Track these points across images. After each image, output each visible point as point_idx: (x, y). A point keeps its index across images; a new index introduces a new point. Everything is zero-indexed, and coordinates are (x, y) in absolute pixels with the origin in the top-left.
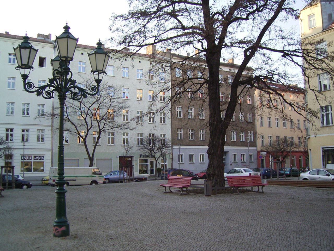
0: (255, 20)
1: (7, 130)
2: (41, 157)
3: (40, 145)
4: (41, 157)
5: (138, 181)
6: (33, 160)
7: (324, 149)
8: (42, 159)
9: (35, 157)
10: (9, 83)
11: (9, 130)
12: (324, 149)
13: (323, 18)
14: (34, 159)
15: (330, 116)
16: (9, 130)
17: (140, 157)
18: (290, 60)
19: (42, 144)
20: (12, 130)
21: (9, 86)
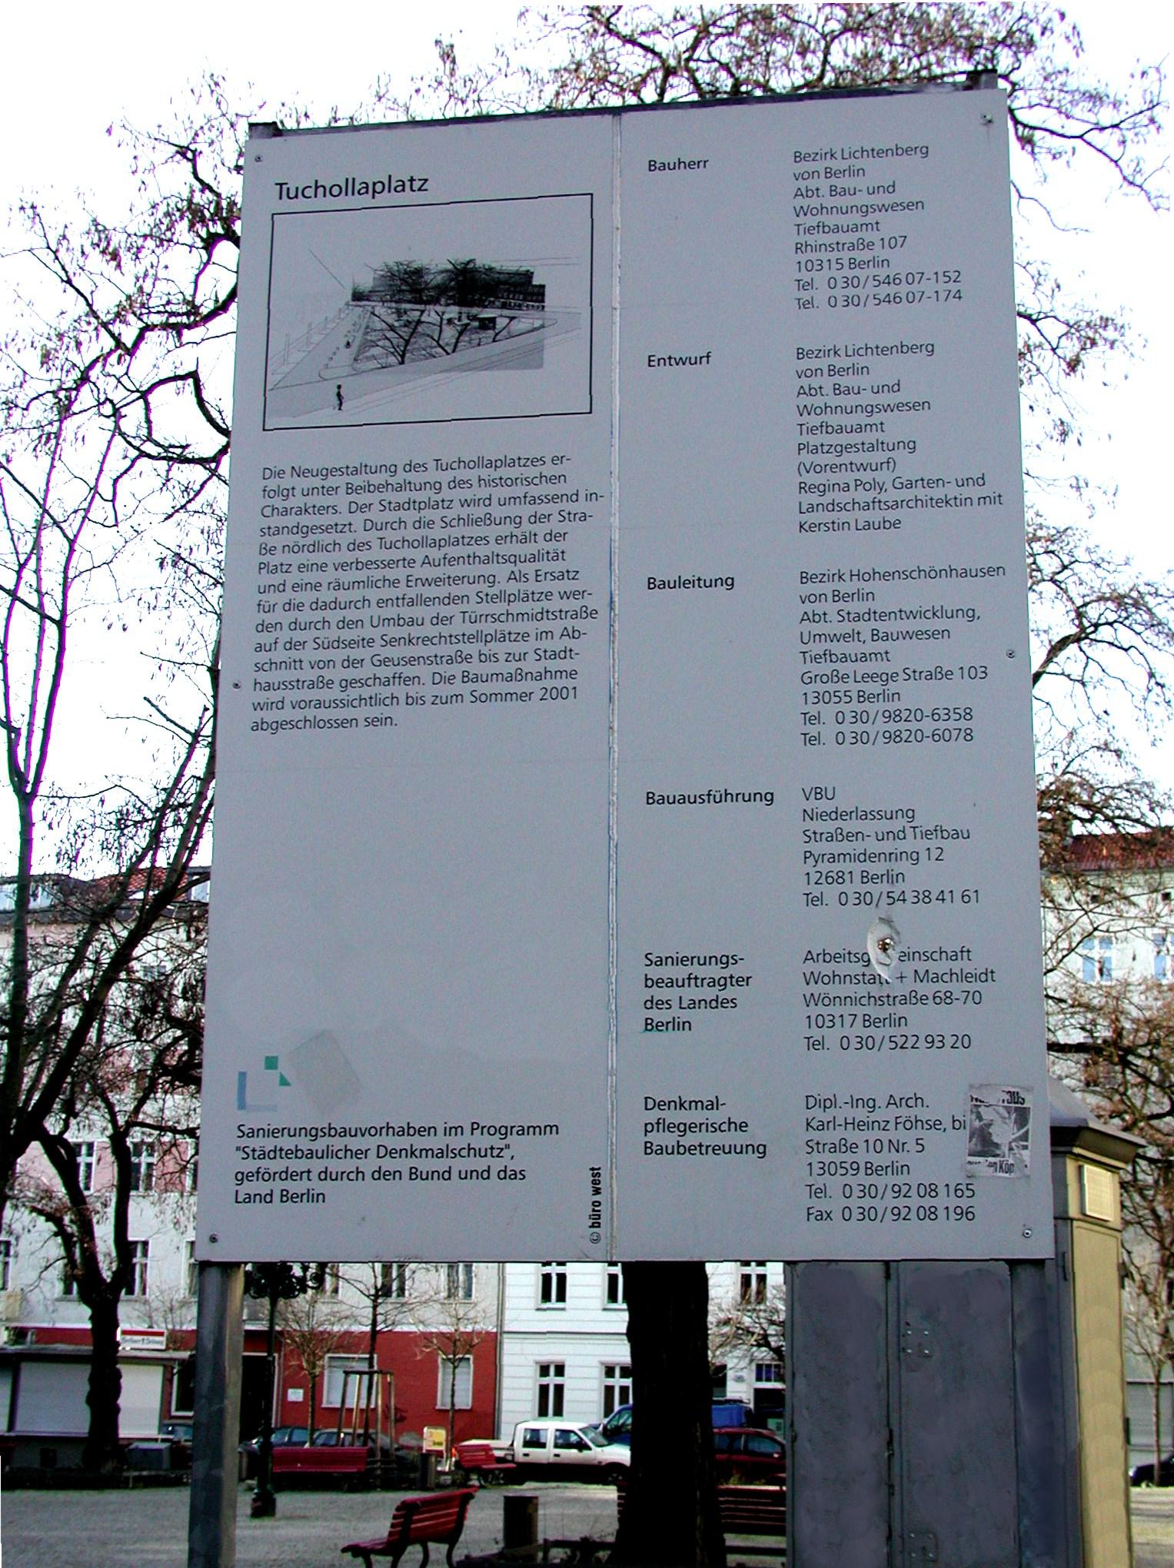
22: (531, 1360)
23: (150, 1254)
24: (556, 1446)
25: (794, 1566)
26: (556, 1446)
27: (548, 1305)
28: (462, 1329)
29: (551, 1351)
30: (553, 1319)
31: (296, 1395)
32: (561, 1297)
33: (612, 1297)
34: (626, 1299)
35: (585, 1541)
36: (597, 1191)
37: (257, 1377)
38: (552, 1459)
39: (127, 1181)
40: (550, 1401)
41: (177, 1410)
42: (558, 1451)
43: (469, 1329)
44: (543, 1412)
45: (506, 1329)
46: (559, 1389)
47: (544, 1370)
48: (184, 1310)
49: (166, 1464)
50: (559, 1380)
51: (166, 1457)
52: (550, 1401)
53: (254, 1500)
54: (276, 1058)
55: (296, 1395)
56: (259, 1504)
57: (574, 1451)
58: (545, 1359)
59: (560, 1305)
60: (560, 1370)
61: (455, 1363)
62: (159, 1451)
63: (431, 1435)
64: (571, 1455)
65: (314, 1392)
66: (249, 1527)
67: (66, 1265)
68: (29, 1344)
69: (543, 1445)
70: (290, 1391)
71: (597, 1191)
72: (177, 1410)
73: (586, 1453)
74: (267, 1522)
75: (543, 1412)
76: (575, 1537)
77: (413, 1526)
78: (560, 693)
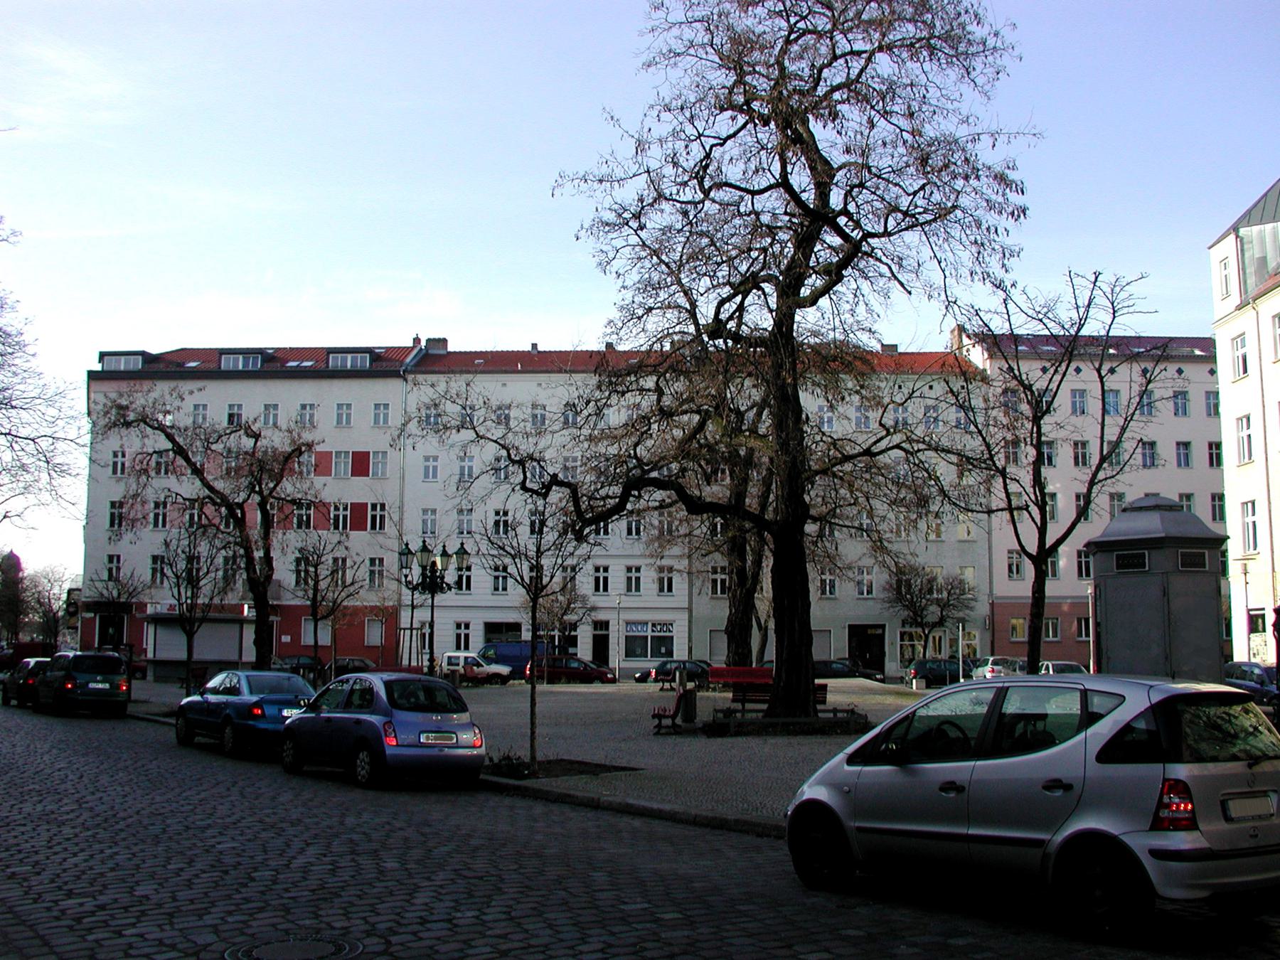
0: (445, 419)
1: (629, 569)
2: (668, 625)
3: (666, 601)
4: (668, 625)
5: (1071, 666)
6: (649, 634)
7: (1260, 621)
8: (670, 631)
9: (654, 625)
10: (427, 468)
11: (601, 570)
12: (1260, 621)
13: (91, 389)
14: (653, 631)
15: (161, 518)
16: (601, 570)
17: (903, 626)
18: (1033, 520)
19: (637, 599)
20: (606, 570)
21: (426, 476)
23: (421, 522)
25: (1276, 757)
31: (286, 639)
39: (267, 523)
44: (458, 648)
47: (458, 626)
50: (467, 631)
52: (462, 642)
55: (286, 639)
58: (459, 620)
60: (467, 626)
65: (296, 637)
67: (977, 368)
68: (1045, 450)
70: (283, 637)
72: (1183, 554)
73: (481, 669)
75: (458, 648)
77: (765, 706)
78: (976, 16)
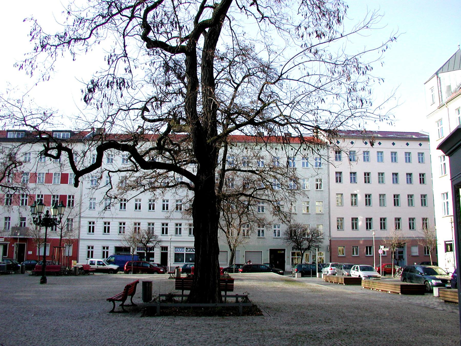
22: (86, 245)
24: (97, 265)
26: (97, 265)
27: (90, 233)
28: (71, 238)
29: (91, 243)
30: (91, 236)
31: (30, 253)
32: (93, 231)
33: (190, 233)
34: (193, 234)
35: (170, 294)
36: (308, 207)
37: (21, 249)
38: (96, 268)
40: (90, 254)
41: (6, 256)
42: (98, 266)
43: (73, 238)
45: (80, 238)
46: (92, 252)
48: (4, 233)
49: (6, 269)
51: (6, 267)
52: (90, 254)
53: (41, 279)
54: (408, 145)
55: (30, 253)
56: (42, 280)
57: (102, 266)
59: (93, 233)
60: (92, 248)
61: (70, 246)
62: (4, 266)
63: (73, 262)
64: (101, 267)
65: (34, 252)
66: (41, 287)
69: (94, 264)
71: (308, 207)
73: (104, 266)
74: (43, 285)
76: (167, 293)
